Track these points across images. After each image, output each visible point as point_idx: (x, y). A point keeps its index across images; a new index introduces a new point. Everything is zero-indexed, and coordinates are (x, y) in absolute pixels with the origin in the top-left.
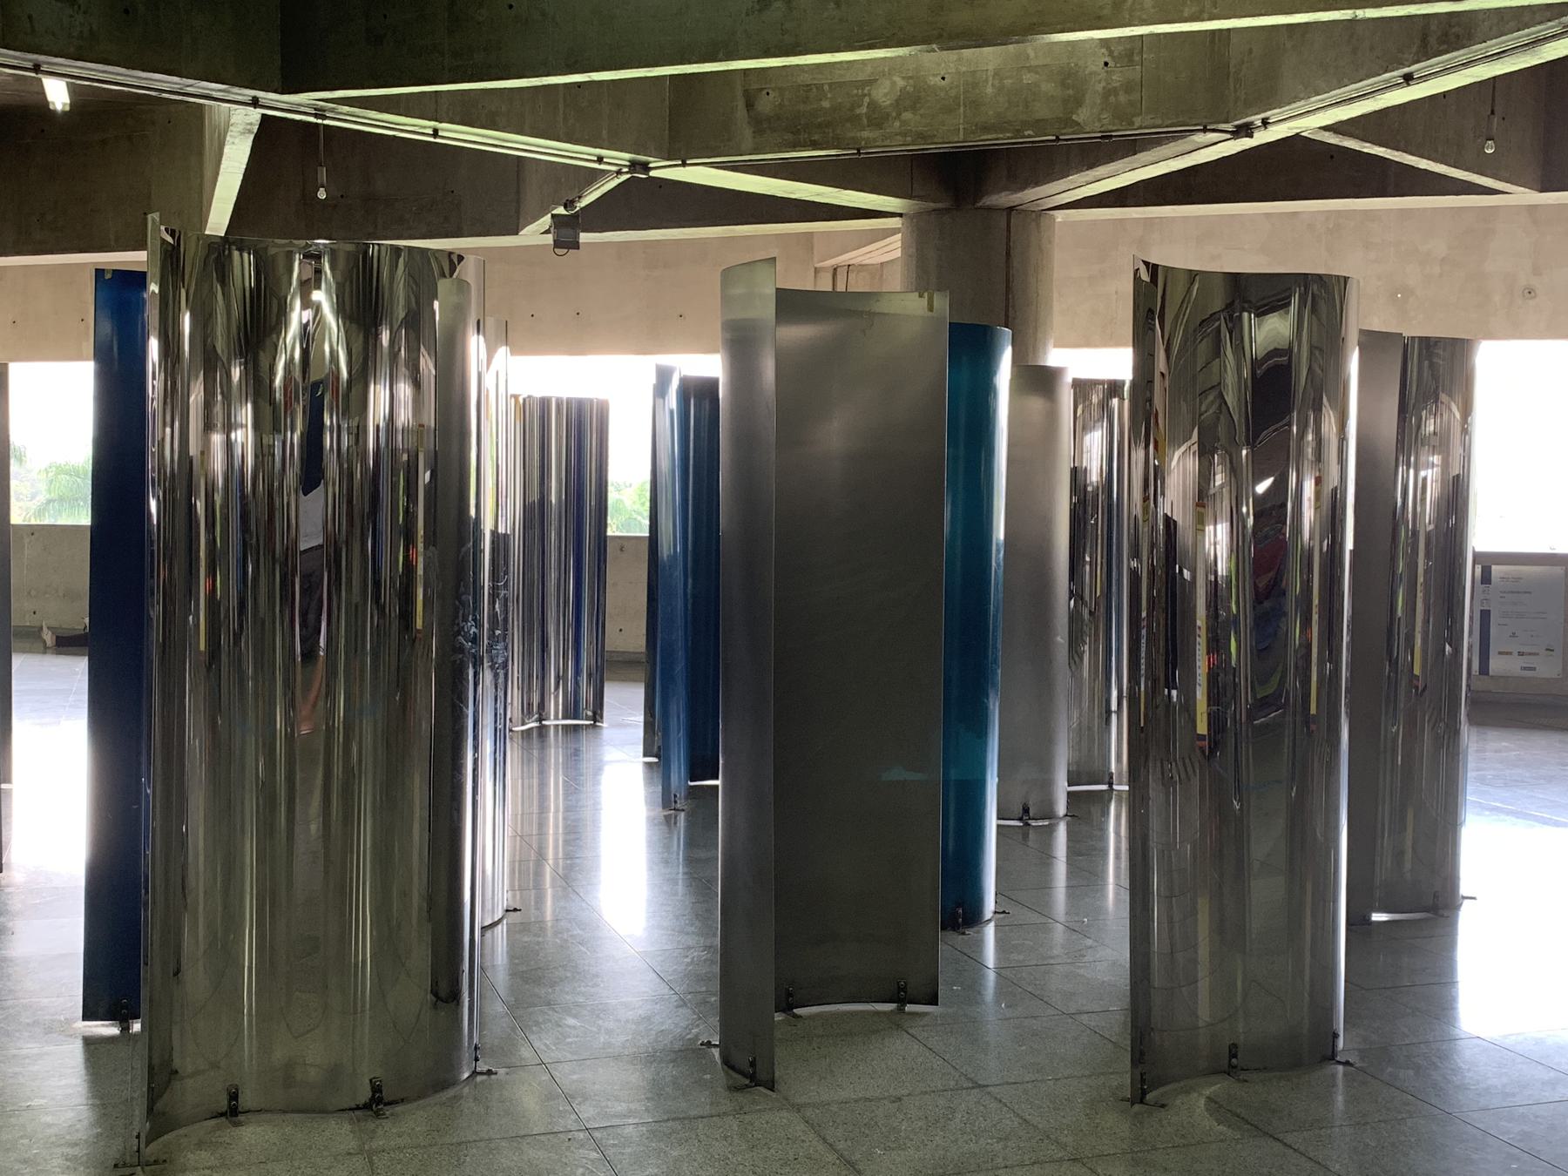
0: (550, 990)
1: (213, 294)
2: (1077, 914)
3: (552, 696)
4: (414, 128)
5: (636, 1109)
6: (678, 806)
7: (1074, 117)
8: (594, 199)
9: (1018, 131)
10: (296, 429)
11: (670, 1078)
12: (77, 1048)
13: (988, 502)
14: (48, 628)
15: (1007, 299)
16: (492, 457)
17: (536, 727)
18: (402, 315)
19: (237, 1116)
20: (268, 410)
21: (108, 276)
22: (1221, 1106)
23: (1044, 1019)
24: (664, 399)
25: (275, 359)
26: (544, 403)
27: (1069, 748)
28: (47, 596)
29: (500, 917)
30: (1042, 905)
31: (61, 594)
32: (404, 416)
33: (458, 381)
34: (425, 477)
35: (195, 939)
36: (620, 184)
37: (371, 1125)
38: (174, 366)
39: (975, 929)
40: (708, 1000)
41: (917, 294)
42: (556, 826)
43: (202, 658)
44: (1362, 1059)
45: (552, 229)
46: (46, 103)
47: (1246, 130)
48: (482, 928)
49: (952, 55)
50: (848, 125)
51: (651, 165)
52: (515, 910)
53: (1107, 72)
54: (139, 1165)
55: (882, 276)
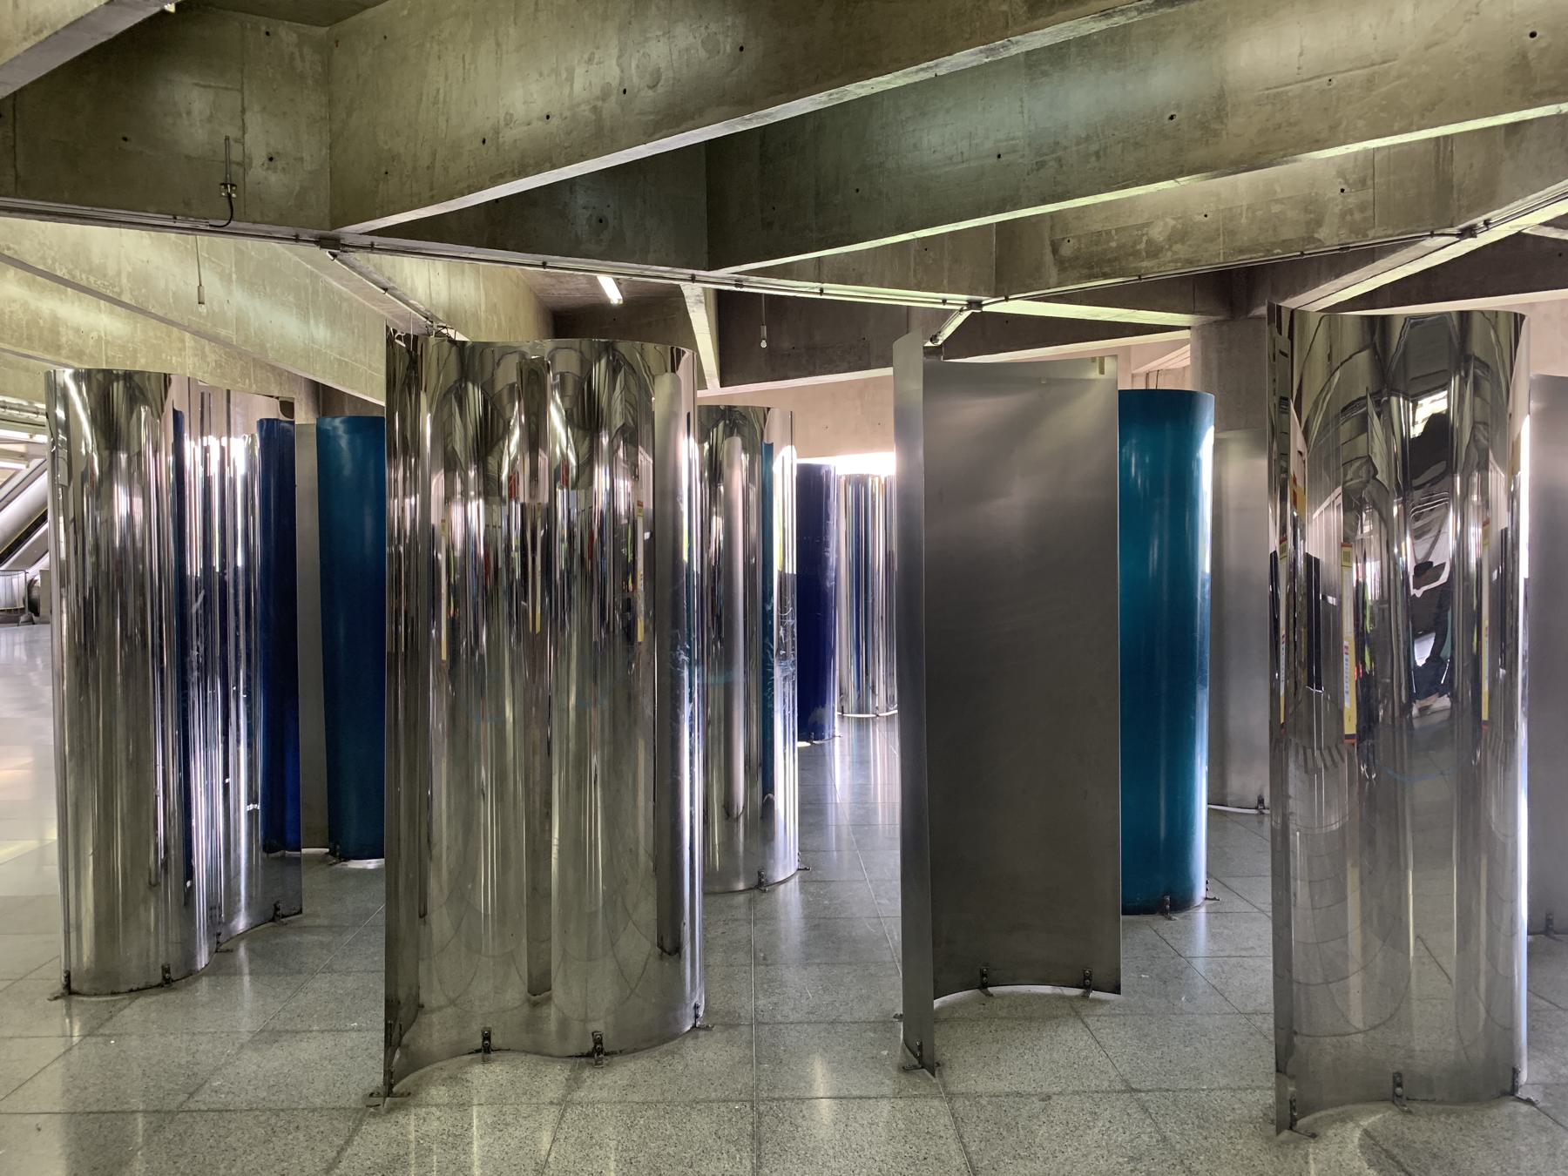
1: (451, 415)
4: (805, 289)
7: (1316, 235)
9: (1268, 250)
19: (489, 1053)
22: (1376, 1144)
39: (1183, 914)
44: (1546, 1095)
47: (1470, 232)
50: (1131, 258)
53: (1344, 197)
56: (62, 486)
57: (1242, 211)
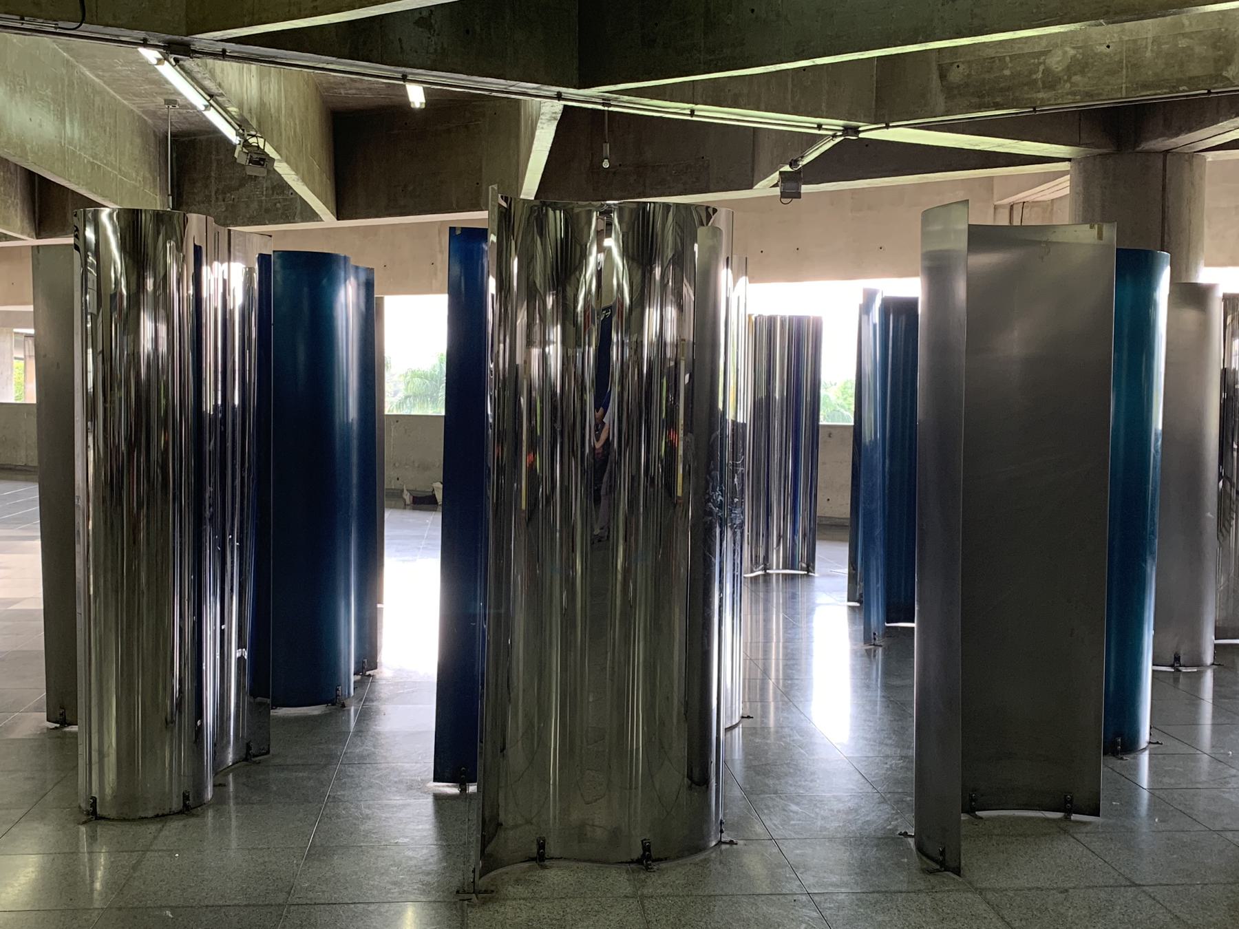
0: (777, 782)
2: (1223, 748)
3: (775, 551)
4: (676, 110)
5: (847, 881)
6: (877, 642)
7: (1224, 74)
8: (813, 158)
9: (1174, 87)
10: (592, 344)
11: (874, 859)
12: (430, 800)
13: (1148, 399)
14: (407, 490)
15: (1163, 227)
16: (733, 363)
17: (762, 575)
18: (670, 256)
19: (544, 861)
20: (571, 329)
21: (458, 232)
23: (1192, 833)
24: (869, 316)
25: (577, 290)
26: (771, 320)
27: (1216, 608)
28: (407, 467)
29: (737, 722)
30: (1192, 740)
31: (416, 465)
32: (670, 335)
33: (711, 303)
34: (685, 379)
35: (516, 725)
36: (835, 145)
37: (642, 876)
38: (506, 298)
39: (1132, 756)
40: (904, 799)
41: (1089, 225)
42: (777, 653)
43: (523, 515)
45: (780, 183)
46: (408, 104)
48: (726, 729)
49: (1116, 28)
51: (860, 129)
52: (749, 717)
54: (474, 893)
55: (1052, 209)
56: (91, 314)
57: (1147, 43)
